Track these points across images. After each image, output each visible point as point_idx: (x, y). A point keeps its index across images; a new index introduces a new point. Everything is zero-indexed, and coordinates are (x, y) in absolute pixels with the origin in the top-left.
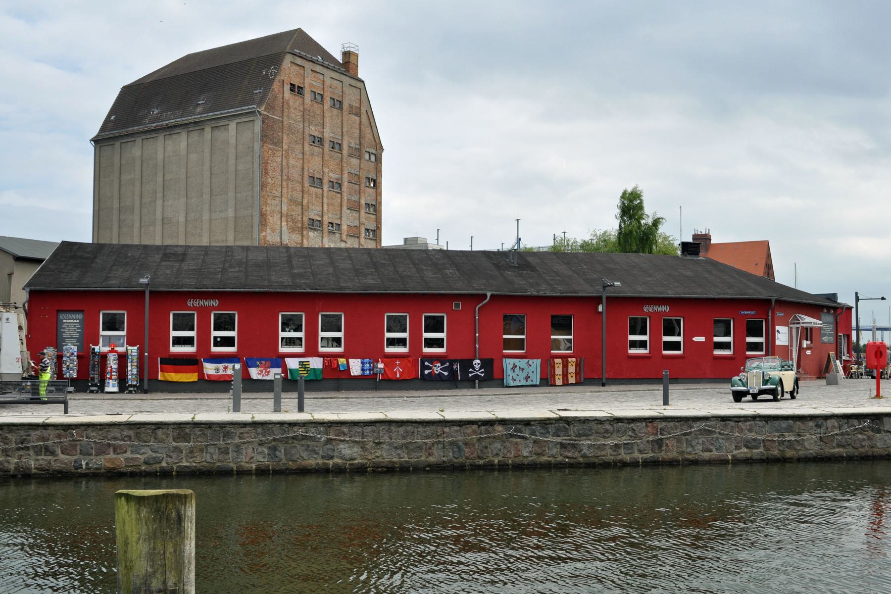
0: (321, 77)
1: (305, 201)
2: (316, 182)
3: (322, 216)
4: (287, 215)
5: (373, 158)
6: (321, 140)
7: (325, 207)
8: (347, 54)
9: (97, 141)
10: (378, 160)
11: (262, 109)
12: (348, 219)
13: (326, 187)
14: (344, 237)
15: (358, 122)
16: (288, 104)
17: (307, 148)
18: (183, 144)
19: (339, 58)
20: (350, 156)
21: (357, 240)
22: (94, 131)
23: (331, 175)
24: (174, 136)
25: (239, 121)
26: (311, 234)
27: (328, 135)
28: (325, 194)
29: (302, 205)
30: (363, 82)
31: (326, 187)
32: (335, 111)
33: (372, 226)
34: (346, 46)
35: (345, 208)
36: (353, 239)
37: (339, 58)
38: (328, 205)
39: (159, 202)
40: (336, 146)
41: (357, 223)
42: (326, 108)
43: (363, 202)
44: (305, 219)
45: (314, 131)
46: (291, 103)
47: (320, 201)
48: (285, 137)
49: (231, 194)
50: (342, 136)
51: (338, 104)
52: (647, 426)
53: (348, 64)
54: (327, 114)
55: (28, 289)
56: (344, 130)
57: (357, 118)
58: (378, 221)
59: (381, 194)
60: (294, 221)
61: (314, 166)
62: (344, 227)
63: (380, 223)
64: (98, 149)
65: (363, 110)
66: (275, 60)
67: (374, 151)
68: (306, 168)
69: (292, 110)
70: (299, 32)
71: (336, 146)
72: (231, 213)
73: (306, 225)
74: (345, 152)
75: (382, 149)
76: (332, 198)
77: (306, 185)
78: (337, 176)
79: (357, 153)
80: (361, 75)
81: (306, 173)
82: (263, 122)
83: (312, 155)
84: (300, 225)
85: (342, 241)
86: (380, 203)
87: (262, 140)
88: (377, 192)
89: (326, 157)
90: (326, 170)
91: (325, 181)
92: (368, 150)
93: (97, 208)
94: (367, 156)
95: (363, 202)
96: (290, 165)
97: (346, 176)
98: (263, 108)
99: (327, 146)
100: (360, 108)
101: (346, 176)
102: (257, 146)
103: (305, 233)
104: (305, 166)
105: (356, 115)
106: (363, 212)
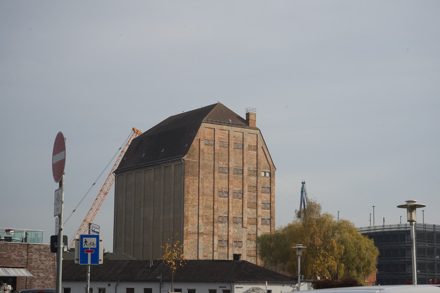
4: (203, 216)
5: (268, 175)
8: (248, 115)
23: (236, 189)
35: (245, 208)
36: (252, 225)
38: (233, 207)
39: (142, 209)
46: (205, 151)
60: (208, 219)
72: (172, 216)
94: (263, 174)
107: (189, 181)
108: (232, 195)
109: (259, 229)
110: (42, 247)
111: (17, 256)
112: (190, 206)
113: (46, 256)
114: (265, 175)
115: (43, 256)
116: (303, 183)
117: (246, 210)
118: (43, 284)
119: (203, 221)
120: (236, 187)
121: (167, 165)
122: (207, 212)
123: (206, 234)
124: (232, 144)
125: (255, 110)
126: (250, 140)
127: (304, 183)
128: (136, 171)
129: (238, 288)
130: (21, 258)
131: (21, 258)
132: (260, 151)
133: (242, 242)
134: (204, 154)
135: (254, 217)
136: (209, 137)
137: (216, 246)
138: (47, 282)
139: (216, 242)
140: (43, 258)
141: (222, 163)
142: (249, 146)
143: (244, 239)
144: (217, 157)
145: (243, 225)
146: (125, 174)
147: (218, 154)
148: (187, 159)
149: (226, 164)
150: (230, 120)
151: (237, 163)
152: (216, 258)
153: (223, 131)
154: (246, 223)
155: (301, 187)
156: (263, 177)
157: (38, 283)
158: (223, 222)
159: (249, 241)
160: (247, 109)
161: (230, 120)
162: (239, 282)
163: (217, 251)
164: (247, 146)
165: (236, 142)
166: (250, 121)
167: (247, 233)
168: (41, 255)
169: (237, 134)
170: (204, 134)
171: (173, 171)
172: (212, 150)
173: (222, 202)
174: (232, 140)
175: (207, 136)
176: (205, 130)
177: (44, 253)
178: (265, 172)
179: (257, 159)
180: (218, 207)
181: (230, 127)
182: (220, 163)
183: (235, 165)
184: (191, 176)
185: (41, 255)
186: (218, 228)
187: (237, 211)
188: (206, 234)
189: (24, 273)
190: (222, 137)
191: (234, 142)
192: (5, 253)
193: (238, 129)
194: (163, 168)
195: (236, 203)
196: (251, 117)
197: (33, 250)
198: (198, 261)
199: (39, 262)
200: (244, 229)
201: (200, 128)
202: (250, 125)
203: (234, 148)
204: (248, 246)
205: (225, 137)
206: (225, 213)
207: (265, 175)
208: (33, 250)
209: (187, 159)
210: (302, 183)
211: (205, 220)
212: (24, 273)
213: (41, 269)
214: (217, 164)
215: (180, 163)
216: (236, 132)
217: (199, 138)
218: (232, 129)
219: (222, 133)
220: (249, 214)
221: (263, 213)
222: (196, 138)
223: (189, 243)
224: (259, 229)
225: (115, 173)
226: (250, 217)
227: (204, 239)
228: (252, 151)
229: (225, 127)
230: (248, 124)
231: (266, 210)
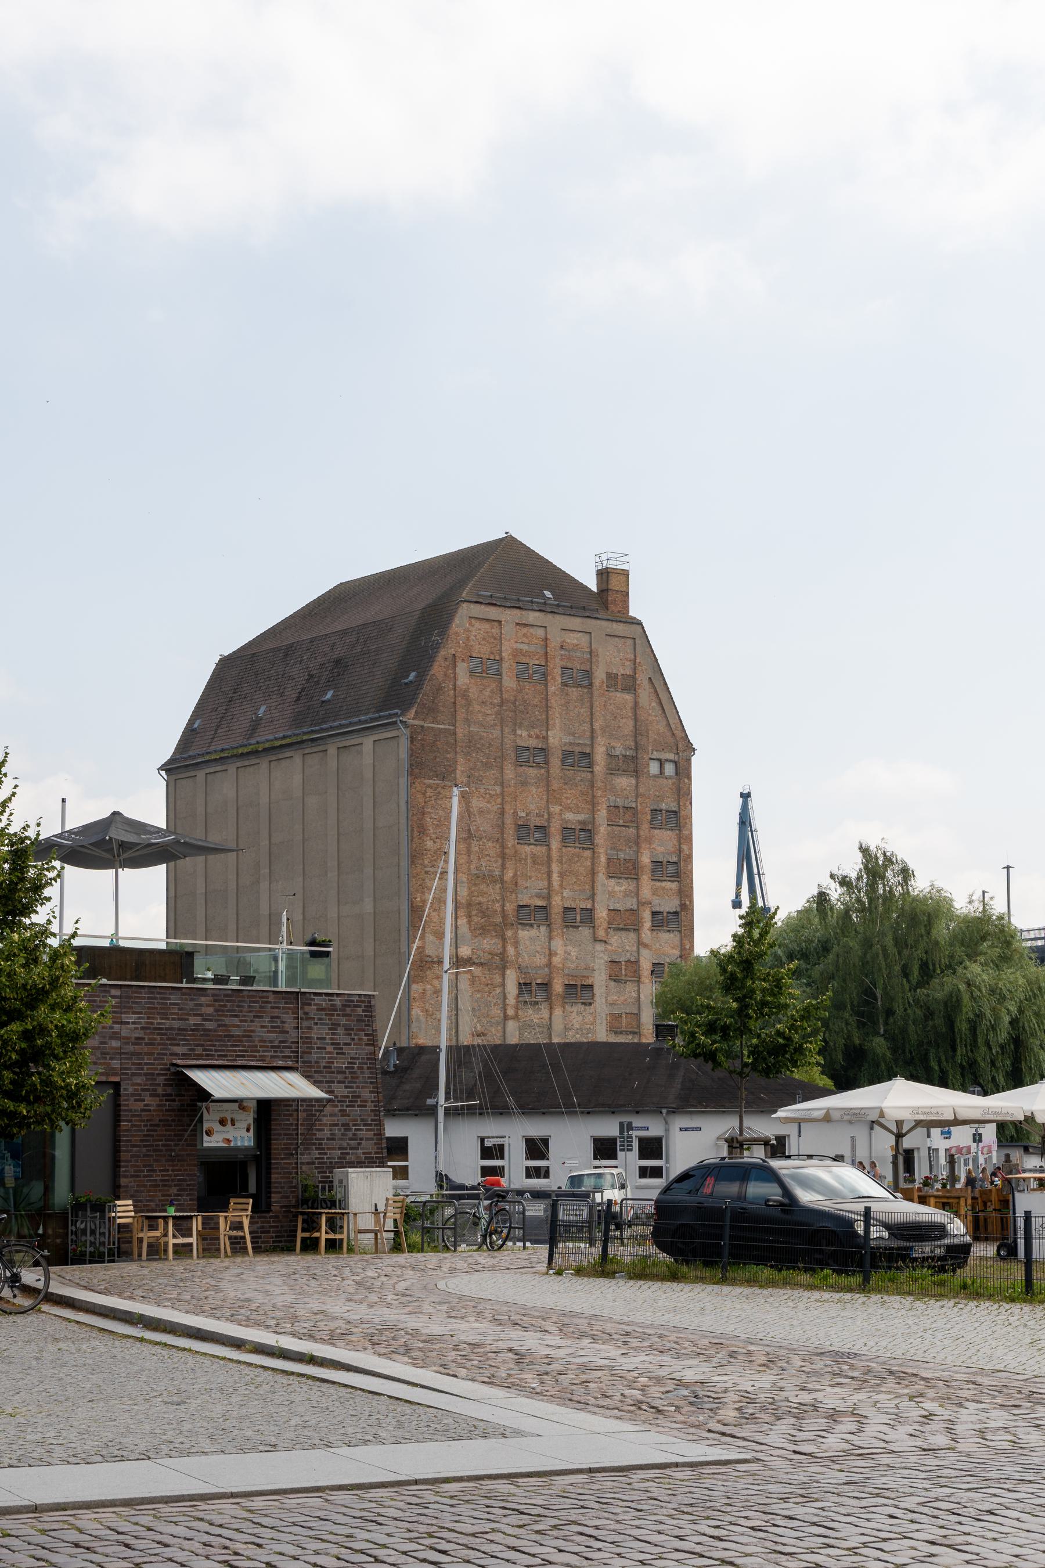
0: (540, 632)
1: (509, 875)
2: (531, 832)
3: (548, 897)
4: (469, 905)
5: (669, 769)
6: (544, 751)
7: (555, 876)
8: (604, 575)
9: (172, 769)
10: (683, 772)
11: (410, 717)
12: (611, 894)
13: (555, 843)
14: (601, 933)
15: (631, 705)
16: (465, 695)
17: (509, 772)
18: (297, 779)
19: (592, 584)
20: (613, 771)
21: (632, 935)
22: (167, 752)
23: (569, 816)
24: (284, 763)
25: (376, 737)
26: (524, 934)
27: (556, 738)
28: (555, 854)
29: (502, 881)
30: (640, 623)
31: (555, 843)
32: (574, 693)
33: (669, 904)
34: (604, 557)
35: (601, 877)
36: (623, 934)
37: (592, 584)
38: (562, 875)
39: (264, 885)
40: (580, 759)
41: (631, 903)
42: (552, 689)
43: (645, 859)
44: (510, 907)
45: (525, 737)
46: (473, 693)
47: (544, 869)
48: (461, 760)
49: (369, 870)
50: (592, 738)
51: (580, 678)
52: (524, 1247)
53: (609, 594)
54: (553, 702)
55: (773, 910)
56: (597, 726)
57: (628, 697)
58: (685, 895)
59: (689, 839)
60: (483, 914)
61: (530, 803)
62: (601, 914)
63: (690, 896)
64: (172, 784)
65: (642, 678)
66: (435, 619)
67: (671, 756)
68: (509, 809)
69: (476, 707)
70: (508, 546)
71: (580, 759)
72: (368, 906)
73: (512, 919)
74: (600, 768)
75: (690, 749)
76: (571, 860)
77: (511, 841)
78: (581, 817)
79: (631, 764)
80: (633, 612)
81: (509, 820)
82: (412, 739)
83: (524, 784)
84: (498, 919)
85: (596, 940)
86: (690, 857)
87: (411, 773)
88: (680, 838)
89: (555, 785)
90: (555, 809)
91: (555, 828)
92: (656, 755)
93: (172, 894)
94: (654, 768)
95: (645, 859)
96: (475, 810)
97: (602, 815)
98: (412, 713)
99: (555, 761)
100: (633, 677)
101: (602, 815)
102: (403, 781)
103: (509, 933)
104: (507, 807)
105: (626, 689)
106: (645, 878)
107: (424, 794)
108: (559, 838)
109: (646, 946)
110: (338, 1002)
111: (268, 1032)
112: (427, 873)
113: (348, 1030)
114: (662, 772)
115: (340, 1030)
116: (746, 796)
117: (603, 885)
118: (344, 1120)
119: (469, 922)
120: (569, 809)
121: (348, 743)
122: (482, 894)
123: (482, 964)
124: (558, 671)
125: (625, 559)
126: (611, 658)
127: (748, 795)
128: (239, 764)
129: (686, 1129)
130: (281, 1038)
131: (281, 1038)
132: (645, 695)
133: (591, 986)
134: (469, 703)
135: (629, 906)
136: (482, 650)
137: (511, 1000)
138: (357, 1111)
139: (512, 989)
140: (342, 1037)
141: (525, 733)
142: (609, 675)
143: (600, 979)
144: (511, 714)
145: (594, 933)
146: (201, 774)
147: (514, 703)
148: (417, 722)
149: (537, 737)
150: (548, 594)
151: (573, 734)
152: (513, 1039)
153: (525, 630)
154: (605, 925)
155: (738, 809)
156: (655, 776)
157: (331, 1115)
158: (531, 925)
159: (613, 983)
160: (598, 556)
161: (548, 594)
162: (691, 1113)
163: (516, 1017)
164: (604, 676)
165: (569, 665)
166: (611, 597)
167: (606, 958)
168: (334, 1026)
169: (572, 639)
170: (468, 638)
171: (368, 760)
172: (492, 692)
173: (529, 861)
174: (554, 657)
175: (477, 647)
176: (469, 625)
177: (343, 1021)
178: (659, 760)
179: (636, 720)
180: (515, 875)
181: (550, 616)
182: (519, 732)
183: (567, 739)
184: (430, 778)
185: (334, 1026)
186: (516, 944)
187: (576, 887)
188: (482, 964)
189: (207, 1081)
190: (525, 647)
191: (563, 663)
192: (236, 1021)
193: (576, 623)
194: (332, 750)
195: (571, 860)
196: (615, 583)
197: (312, 1010)
198: (550, 1046)
199: (330, 1048)
200: (599, 947)
201: (457, 620)
202: (612, 607)
203: (564, 684)
204: (613, 998)
205: (533, 649)
206: (538, 896)
207: (662, 772)
208: (312, 1010)
209: (417, 722)
210: (742, 795)
211: (476, 919)
212: (207, 1081)
213: (339, 1073)
214: (512, 737)
215: (390, 735)
216: (565, 632)
217: (452, 652)
218: (556, 623)
219: (524, 635)
220: (611, 894)
221: (655, 892)
222: (442, 653)
223: (429, 993)
224: (646, 946)
225: (168, 771)
226: (618, 906)
227: (473, 981)
228: (618, 694)
229: (532, 617)
230: (605, 606)
231: (664, 884)
